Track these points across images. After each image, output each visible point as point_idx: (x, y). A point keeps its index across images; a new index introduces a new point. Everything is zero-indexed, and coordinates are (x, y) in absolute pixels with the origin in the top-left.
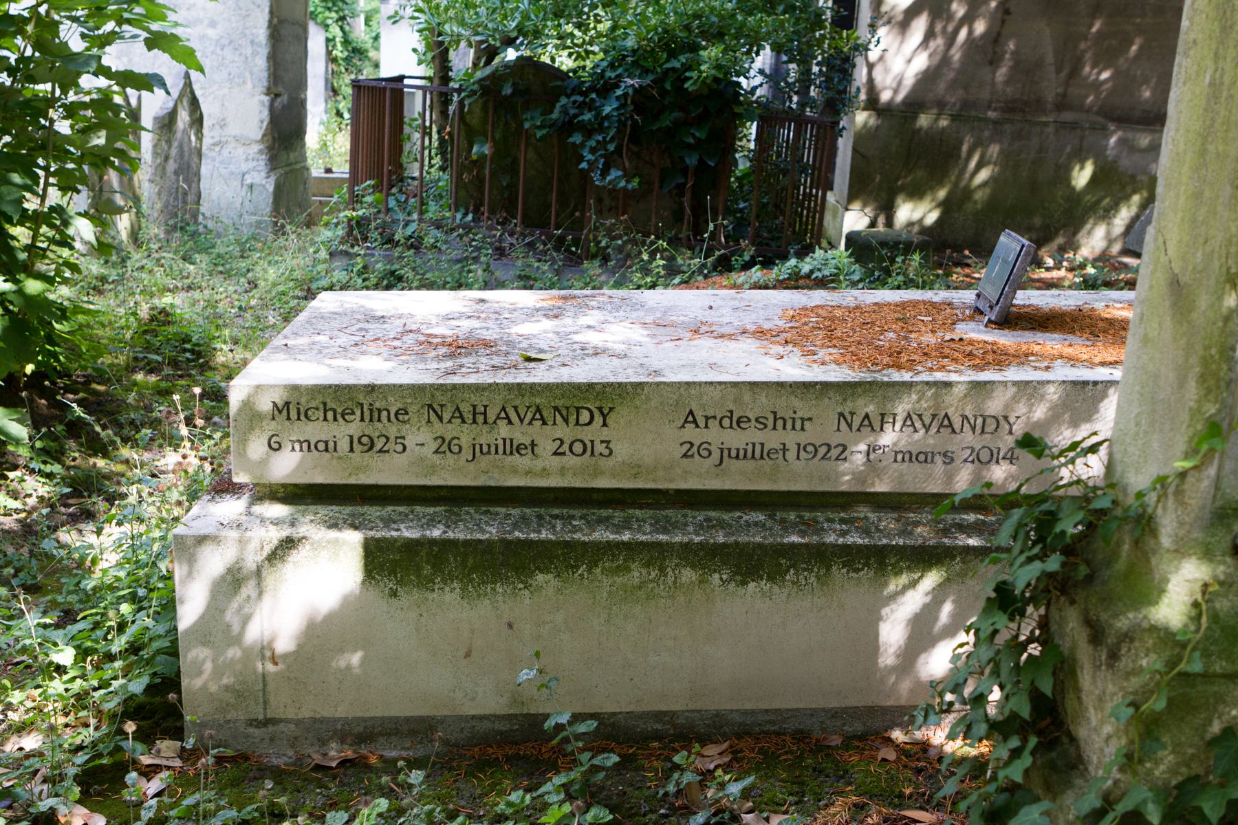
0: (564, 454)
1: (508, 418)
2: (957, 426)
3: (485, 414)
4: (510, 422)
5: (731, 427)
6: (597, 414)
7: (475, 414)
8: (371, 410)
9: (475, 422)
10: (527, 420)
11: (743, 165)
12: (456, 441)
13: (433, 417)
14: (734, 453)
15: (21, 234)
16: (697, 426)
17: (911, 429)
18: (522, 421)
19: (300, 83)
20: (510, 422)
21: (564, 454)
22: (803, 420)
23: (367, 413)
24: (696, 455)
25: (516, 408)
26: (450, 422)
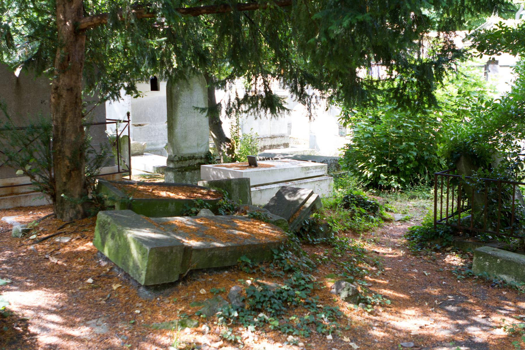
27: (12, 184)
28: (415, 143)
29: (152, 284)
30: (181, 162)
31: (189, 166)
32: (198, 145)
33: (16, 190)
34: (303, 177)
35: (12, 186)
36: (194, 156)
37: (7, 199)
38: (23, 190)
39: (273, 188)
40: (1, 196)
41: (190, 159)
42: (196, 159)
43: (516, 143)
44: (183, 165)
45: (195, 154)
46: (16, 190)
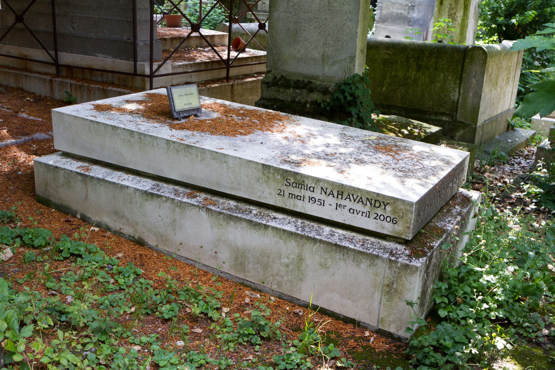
0: (377, 219)
1: (350, 198)
2: (365, 203)
3: (342, 195)
4: (350, 200)
5: (296, 187)
6: (382, 203)
7: (338, 194)
8: (307, 186)
9: (337, 197)
10: (357, 200)
11: (213, 86)
12: (395, 219)
13: (323, 193)
14: (364, 215)
15: (542, 173)
16: (334, 197)
17: (349, 200)
18: (355, 201)
19: (16, 70)
20: (350, 200)
21: (377, 219)
22: (375, 200)
23: (306, 187)
24: (379, 219)
25: (353, 195)
26: (358, 202)
27: (26, 56)
28: (19, 269)
29: (242, 277)
30: (275, 88)
31: (293, 101)
32: (324, 58)
33: (30, 65)
34: (271, 202)
35: (25, 59)
36: (310, 82)
37: (10, 73)
38: (37, 67)
39: (123, 187)
40: (3, 67)
41: (297, 88)
42: (311, 91)
43: (549, 16)
44: (280, 97)
45: (316, 78)
46: (30, 65)
